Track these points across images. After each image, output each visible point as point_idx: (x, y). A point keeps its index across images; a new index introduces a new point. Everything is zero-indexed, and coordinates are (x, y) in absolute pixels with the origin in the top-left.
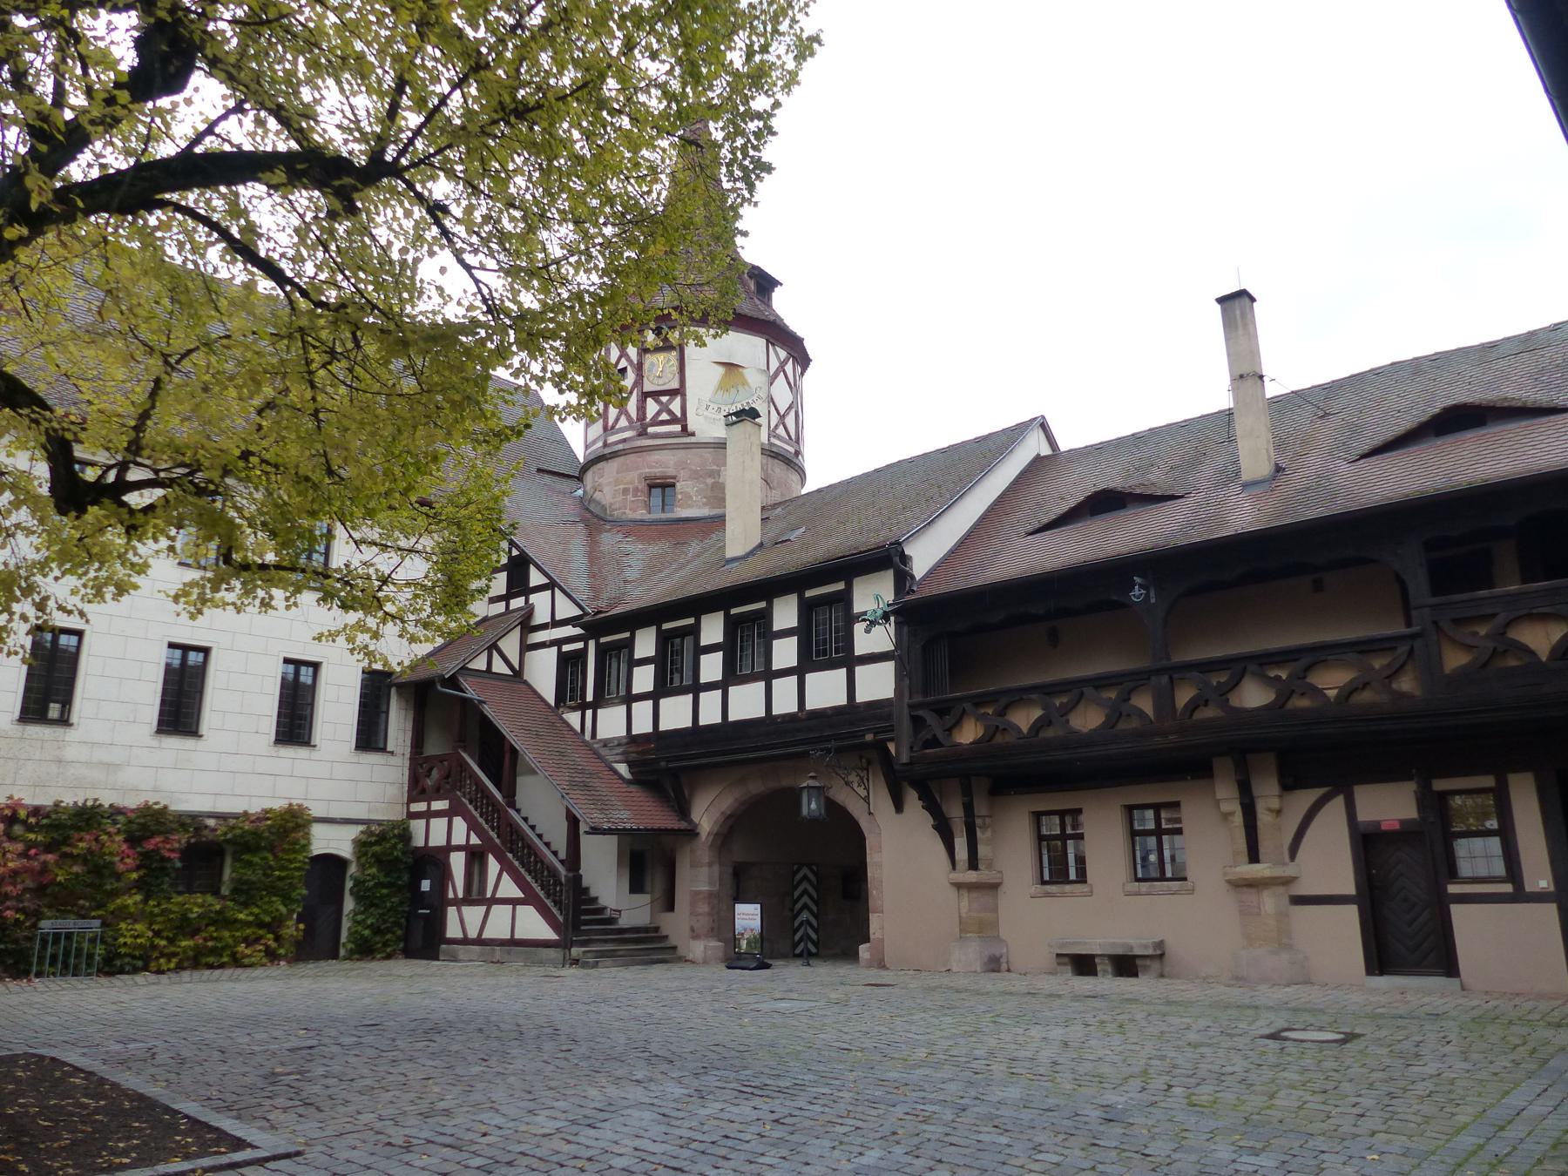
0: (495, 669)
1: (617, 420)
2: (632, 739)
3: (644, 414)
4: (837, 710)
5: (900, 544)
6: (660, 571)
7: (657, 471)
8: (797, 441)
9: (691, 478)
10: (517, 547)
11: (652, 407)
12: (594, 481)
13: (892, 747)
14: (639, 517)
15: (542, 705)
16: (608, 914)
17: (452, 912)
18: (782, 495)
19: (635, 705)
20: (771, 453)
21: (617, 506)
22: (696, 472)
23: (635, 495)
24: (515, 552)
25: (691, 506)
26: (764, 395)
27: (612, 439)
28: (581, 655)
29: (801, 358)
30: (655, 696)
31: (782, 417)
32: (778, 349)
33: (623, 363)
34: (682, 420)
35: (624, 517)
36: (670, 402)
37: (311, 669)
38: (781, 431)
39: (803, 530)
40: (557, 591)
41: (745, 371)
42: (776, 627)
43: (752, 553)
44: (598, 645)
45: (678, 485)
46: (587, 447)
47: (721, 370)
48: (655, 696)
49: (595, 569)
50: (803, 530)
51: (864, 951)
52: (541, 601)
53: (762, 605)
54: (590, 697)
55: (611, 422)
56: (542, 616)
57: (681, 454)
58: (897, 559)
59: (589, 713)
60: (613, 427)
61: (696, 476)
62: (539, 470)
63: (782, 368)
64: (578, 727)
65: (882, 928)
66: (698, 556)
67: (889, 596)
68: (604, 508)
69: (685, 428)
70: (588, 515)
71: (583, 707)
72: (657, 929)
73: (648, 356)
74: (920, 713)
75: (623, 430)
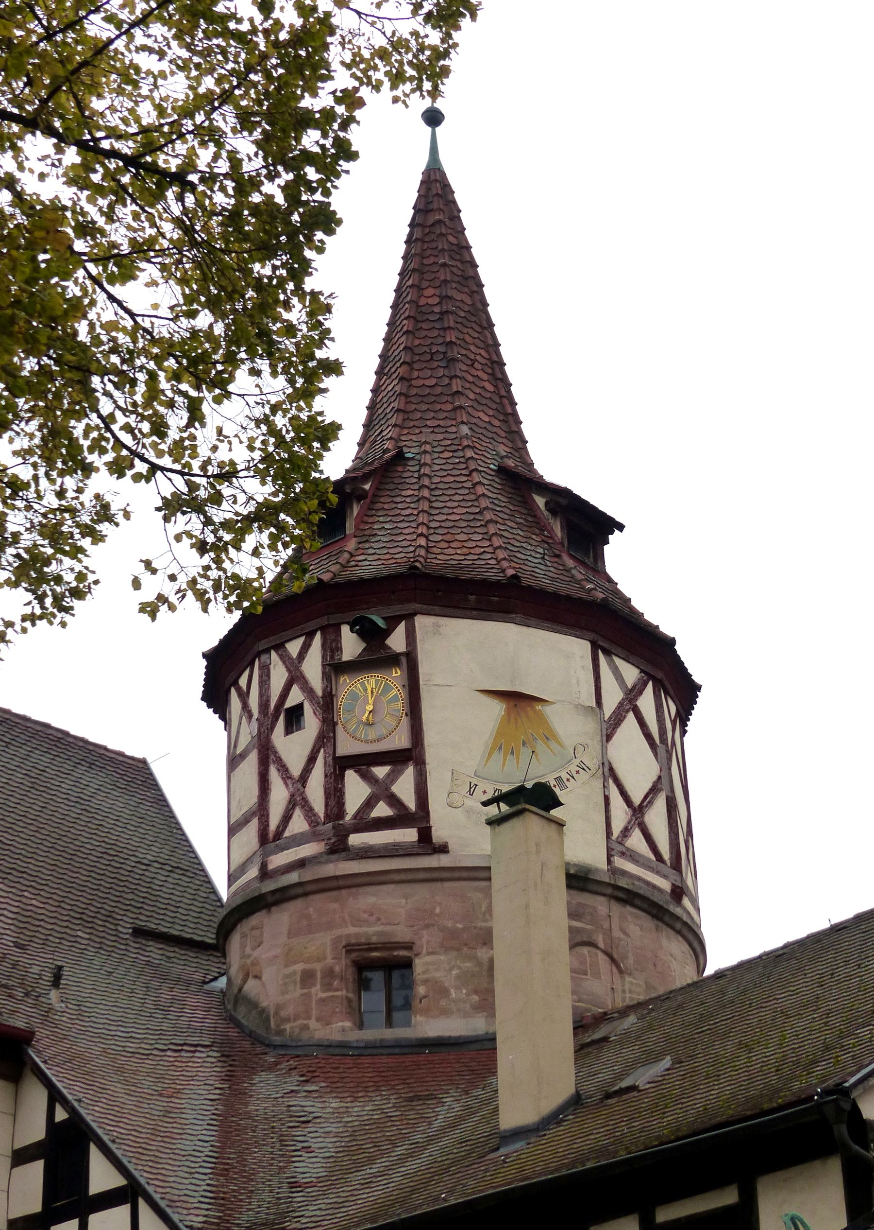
1: (286, 818)
3: (341, 804)
5: (845, 1093)
6: (371, 1160)
7: (371, 931)
8: (676, 865)
10: (65, 1103)
12: (244, 956)
14: (337, 1037)
18: (648, 986)
21: (289, 1011)
22: (453, 934)
23: (327, 986)
24: (61, 1115)
25: (445, 1012)
26: (593, 762)
27: (278, 860)
31: (638, 811)
32: (618, 662)
33: (296, 696)
35: (305, 1036)
36: (393, 777)
39: (667, 1062)
41: (547, 710)
43: (554, 1119)
47: (497, 708)
49: (231, 1154)
50: (667, 1062)
55: (274, 822)
57: (421, 893)
58: (842, 1131)
60: (279, 834)
62: (139, 933)
66: (453, 1126)
68: (263, 1015)
69: (425, 835)
70: (233, 1033)
73: (344, 679)
75: (299, 840)
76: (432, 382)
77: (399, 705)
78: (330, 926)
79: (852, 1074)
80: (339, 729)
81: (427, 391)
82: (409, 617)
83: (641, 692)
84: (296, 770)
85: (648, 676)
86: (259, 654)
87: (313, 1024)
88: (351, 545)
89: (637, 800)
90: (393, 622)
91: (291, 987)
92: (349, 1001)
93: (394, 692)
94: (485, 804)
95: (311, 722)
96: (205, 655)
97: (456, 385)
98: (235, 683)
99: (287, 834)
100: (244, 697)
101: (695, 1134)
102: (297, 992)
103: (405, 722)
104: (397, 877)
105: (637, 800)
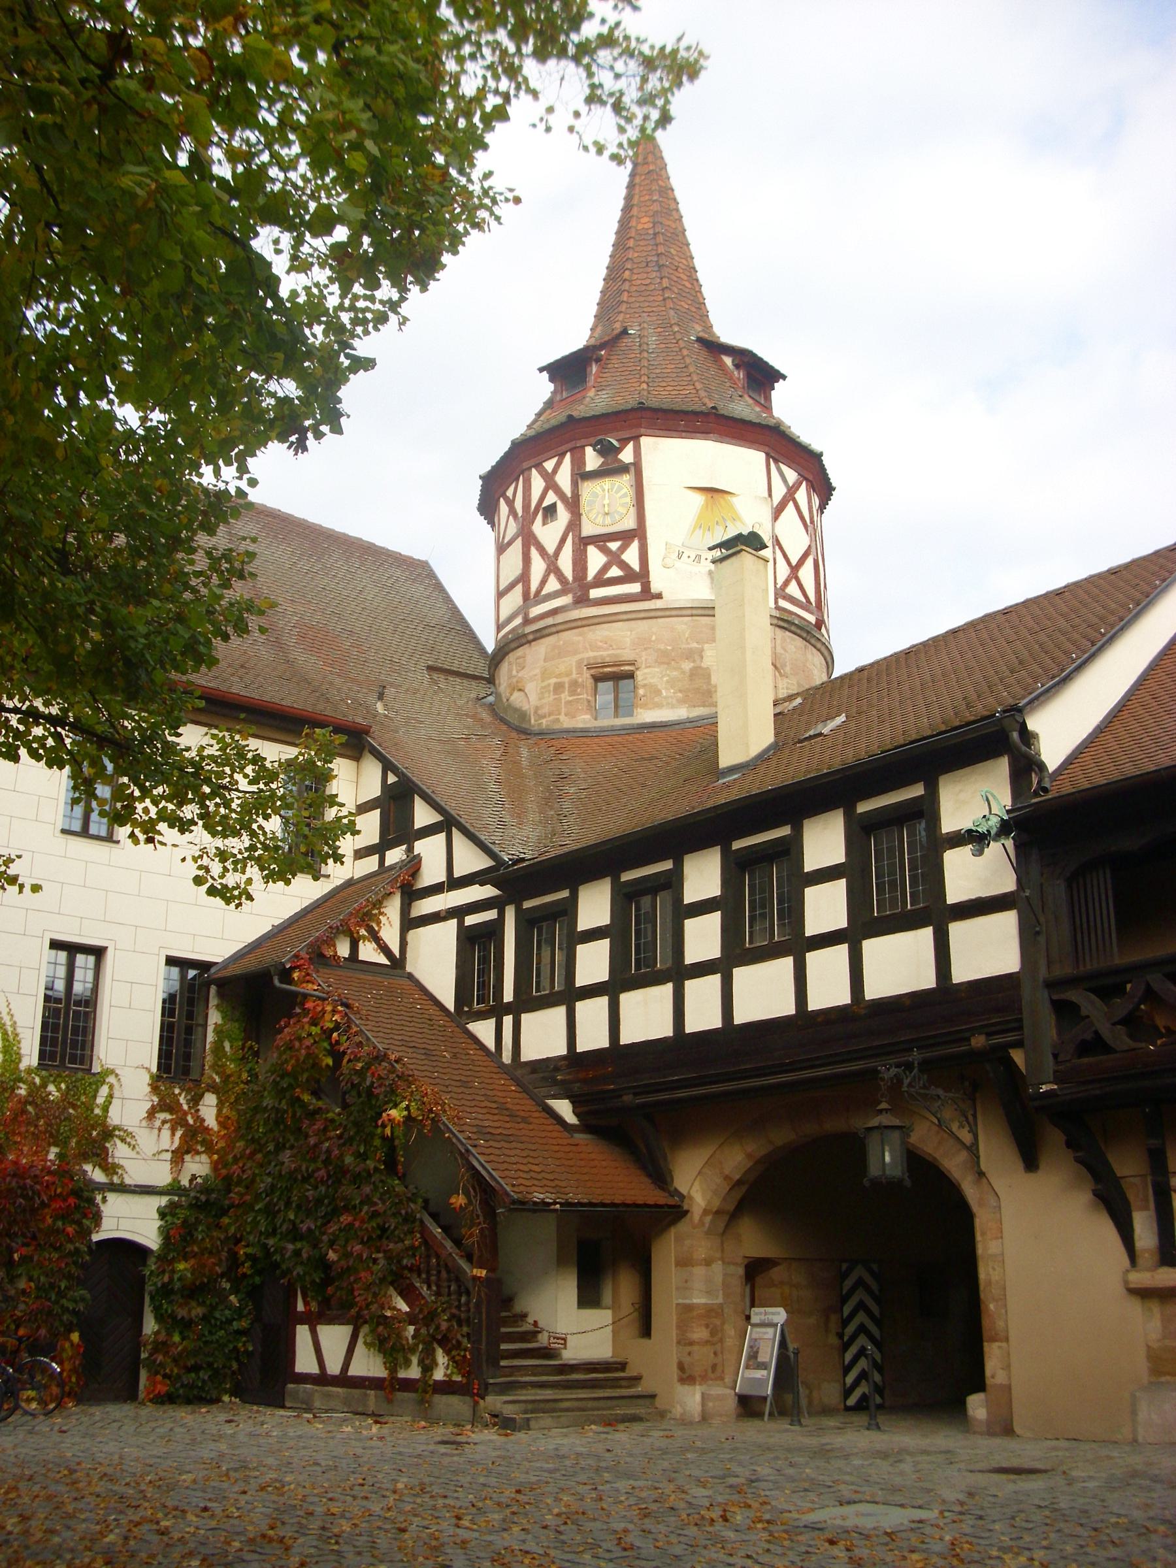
0: (362, 956)
1: (544, 582)
2: (575, 1059)
3: (584, 569)
4: (917, 999)
7: (605, 654)
9: (659, 663)
10: (395, 770)
11: (595, 559)
13: (1018, 1056)
15: (433, 1010)
16: (543, 1340)
17: (302, 1333)
19: (579, 1005)
20: (784, 622)
21: (546, 710)
23: (573, 692)
24: (392, 778)
25: (659, 706)
27: (535, 611)
28: (493, 931)
29: (823, 488)
30: (612, 989)
31: (795, 569)
32: (784, 467)
33: (551, 498)
34: (642, 576)
35: (556, 727)
36: (623, 549)
37: (91, 959)
38: (793, 589)
40: (457, 835)
41: (734, 500)
42: (810, 865)
44: (519, 912)
45: (639, 675)
46: (499, 628)
47: (699, 499)
48: (612, 989)
50: (842, 718)
51: (977, 1406)
52: (431, 850)
53: (785, 831)
54: (508, 996)
56: (432, 872)
59: (508, 1021)
61: (665, 659)
63: (790, 496)
64: (490, 1044)
65: (1007, 1367)
67: (1003, 799)
68: (523, 716)
71: (497, 1011)
72: (623, 1366)
74: (1073, 995)
76: (648, 281)
77: (628, 500)
78: (575, 652)
79: (1024, 697)
80: (584, 518)
81: (644, 288)
82: (636, 438)
83: (797, 489)
84: (551, 550)
85: (803, 477)
86: (522, 472)
87: (562, 718)
88: (591, 393)
89: (794, 562)
90: (624, 442)
91: (546, 695)
92: (589, 701)
93: (625, 490)
94: (710, 549)
95: (563, 515)
96: (481, 477)
97: (665, 283)
98: (504, 495)
99: (543, 593)
100: (510, 503)
101: (896, 748)
102: (550, 698)
103: (633, 511)
104: (625, 617)
105: (794, 563)
